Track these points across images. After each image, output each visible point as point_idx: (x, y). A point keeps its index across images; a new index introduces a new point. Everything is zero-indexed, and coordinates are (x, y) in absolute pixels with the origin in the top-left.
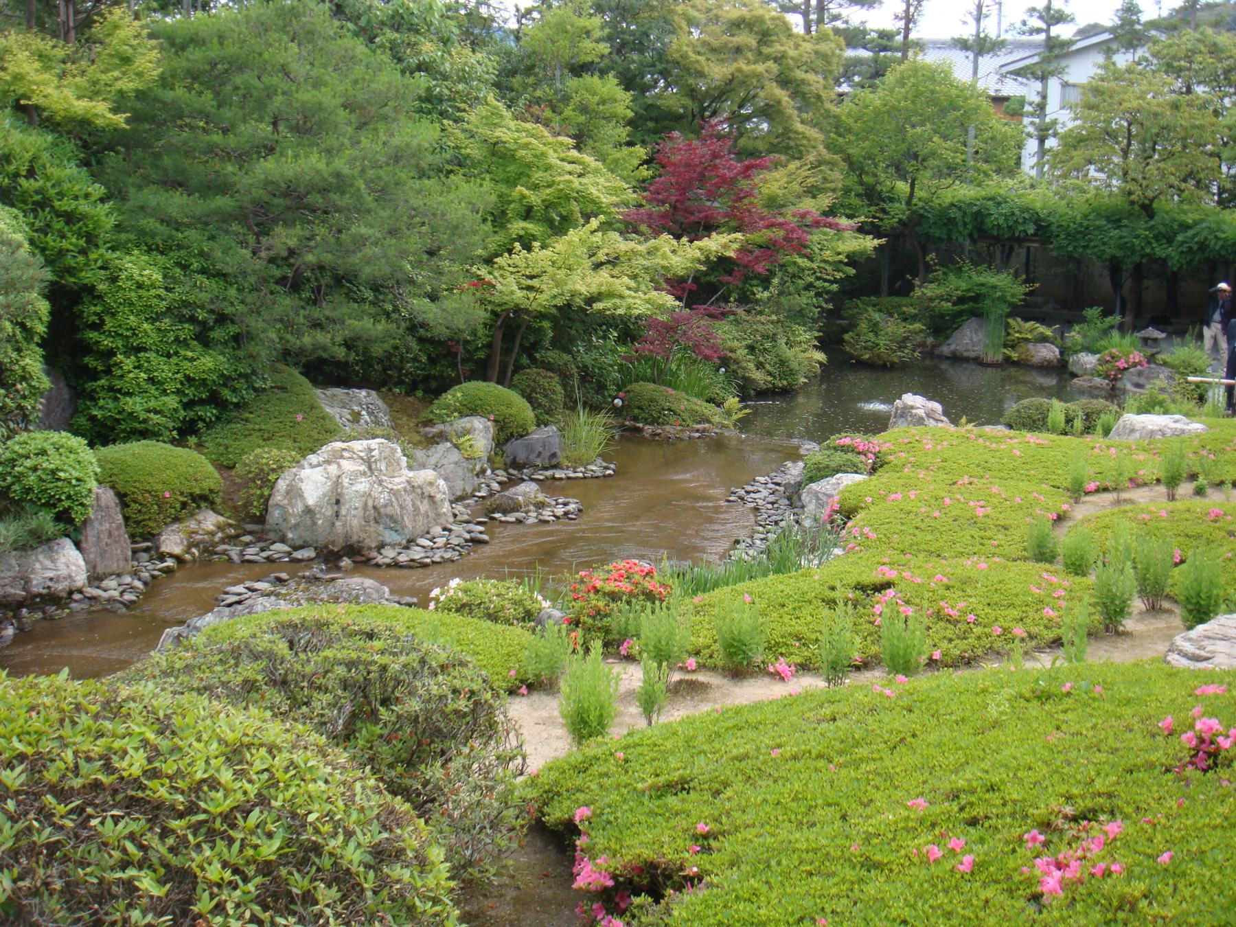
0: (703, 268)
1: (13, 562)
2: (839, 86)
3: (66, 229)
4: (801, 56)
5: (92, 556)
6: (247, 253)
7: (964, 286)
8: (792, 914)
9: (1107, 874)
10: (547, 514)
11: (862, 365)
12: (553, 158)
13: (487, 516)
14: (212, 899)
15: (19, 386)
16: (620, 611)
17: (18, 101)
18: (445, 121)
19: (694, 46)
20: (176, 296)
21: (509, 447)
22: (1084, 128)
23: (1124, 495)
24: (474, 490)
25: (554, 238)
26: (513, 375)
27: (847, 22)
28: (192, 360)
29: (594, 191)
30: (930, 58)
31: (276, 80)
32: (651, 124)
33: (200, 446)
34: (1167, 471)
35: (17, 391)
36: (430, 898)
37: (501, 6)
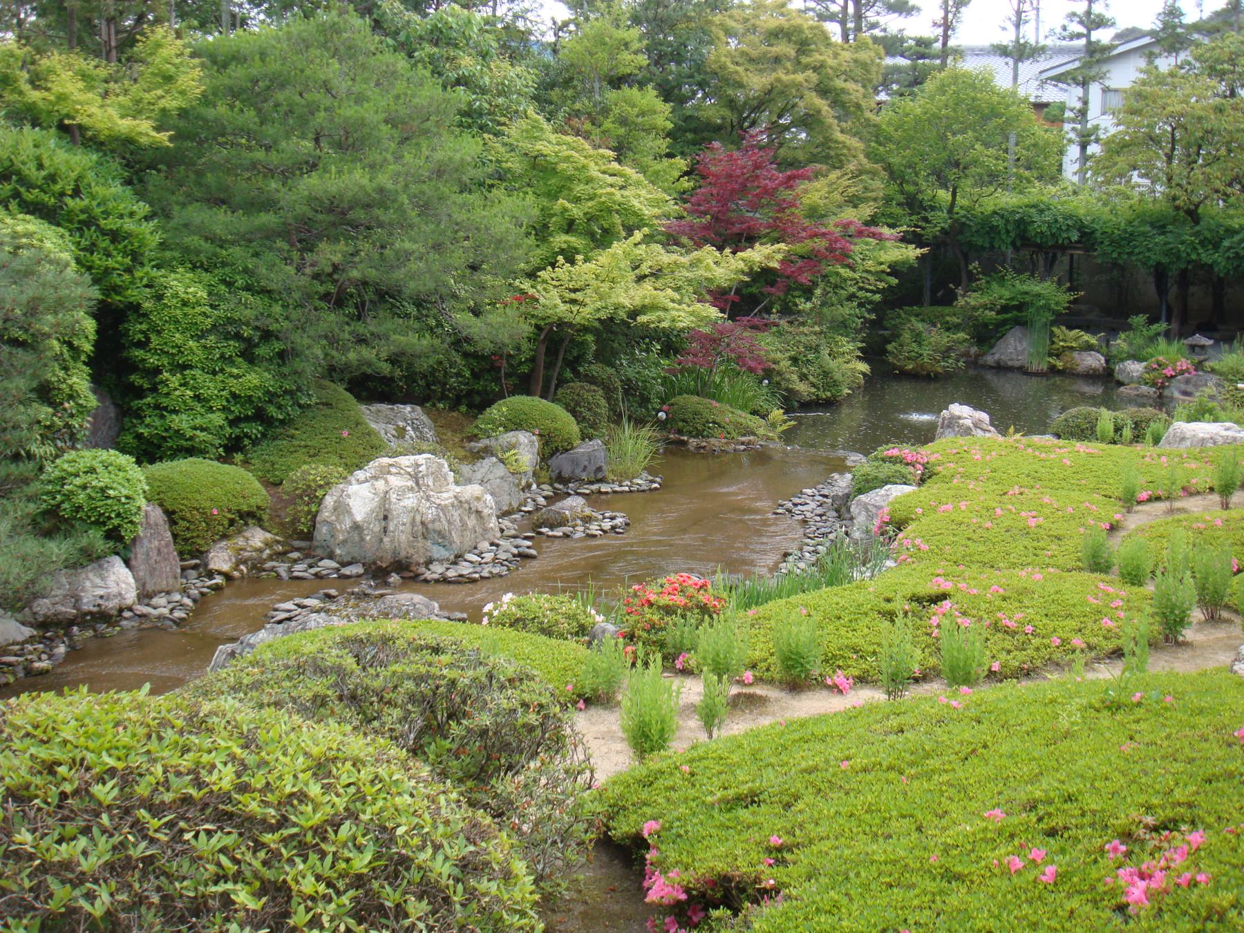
0: (747, 279)
1: (64, 580)
2: (878, 94)
3: (112, 247)
4: (840, 65)
5: (141, 574)
6: (291, 269)
7: (1007, 294)
8: (875, 925)
9: (1193, 884)
10: (594, 528)
11: (905, 375)
12: (594, 171)
13: (534, 531)
14: (307, 912)
15: (67, 405)
16: (675, 625)
17: (61, 121)
18: (486, 136)
19: (732, 57)
20: (221, 313)
21: (554, 462)
22: (1127, 133)
23: (1177, 504)
24: (520, 505)
25: (596, 251)
26: (556, 389)
27: (885, 30)
28: (237, 377)
29: (635, 203)
30: (970, 65)
31: (317, 96)
32: (690, 136)
33: (246, 462)
34: (1221, 479)
35: (65, 410)
36: (516, 911)
37: (539, 20)
